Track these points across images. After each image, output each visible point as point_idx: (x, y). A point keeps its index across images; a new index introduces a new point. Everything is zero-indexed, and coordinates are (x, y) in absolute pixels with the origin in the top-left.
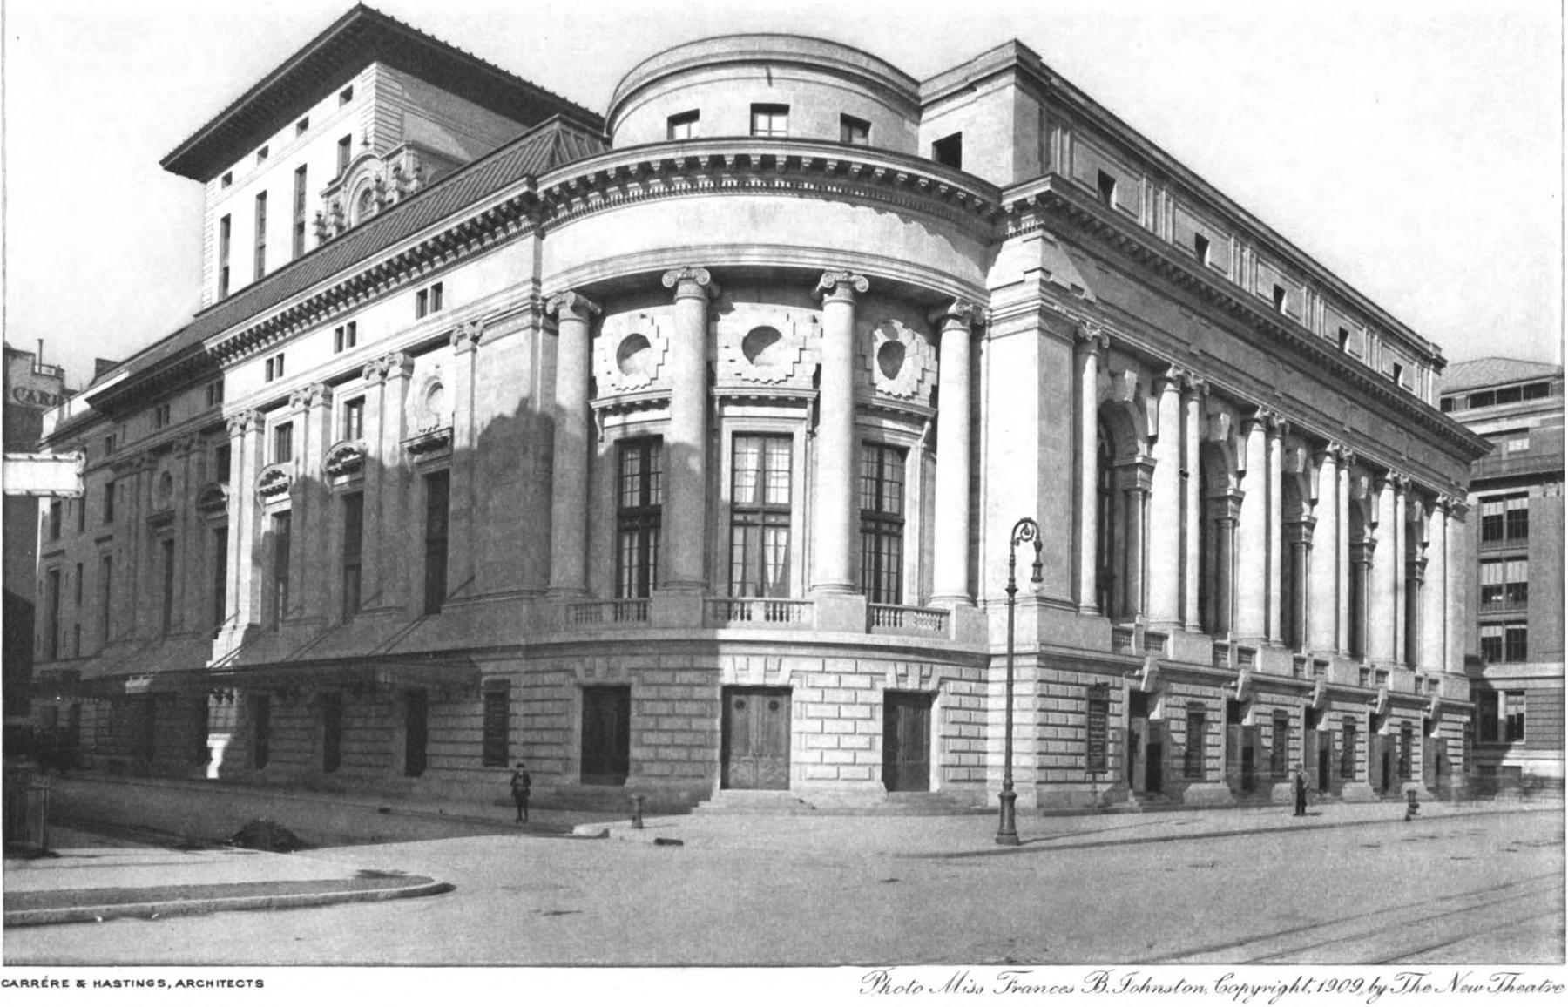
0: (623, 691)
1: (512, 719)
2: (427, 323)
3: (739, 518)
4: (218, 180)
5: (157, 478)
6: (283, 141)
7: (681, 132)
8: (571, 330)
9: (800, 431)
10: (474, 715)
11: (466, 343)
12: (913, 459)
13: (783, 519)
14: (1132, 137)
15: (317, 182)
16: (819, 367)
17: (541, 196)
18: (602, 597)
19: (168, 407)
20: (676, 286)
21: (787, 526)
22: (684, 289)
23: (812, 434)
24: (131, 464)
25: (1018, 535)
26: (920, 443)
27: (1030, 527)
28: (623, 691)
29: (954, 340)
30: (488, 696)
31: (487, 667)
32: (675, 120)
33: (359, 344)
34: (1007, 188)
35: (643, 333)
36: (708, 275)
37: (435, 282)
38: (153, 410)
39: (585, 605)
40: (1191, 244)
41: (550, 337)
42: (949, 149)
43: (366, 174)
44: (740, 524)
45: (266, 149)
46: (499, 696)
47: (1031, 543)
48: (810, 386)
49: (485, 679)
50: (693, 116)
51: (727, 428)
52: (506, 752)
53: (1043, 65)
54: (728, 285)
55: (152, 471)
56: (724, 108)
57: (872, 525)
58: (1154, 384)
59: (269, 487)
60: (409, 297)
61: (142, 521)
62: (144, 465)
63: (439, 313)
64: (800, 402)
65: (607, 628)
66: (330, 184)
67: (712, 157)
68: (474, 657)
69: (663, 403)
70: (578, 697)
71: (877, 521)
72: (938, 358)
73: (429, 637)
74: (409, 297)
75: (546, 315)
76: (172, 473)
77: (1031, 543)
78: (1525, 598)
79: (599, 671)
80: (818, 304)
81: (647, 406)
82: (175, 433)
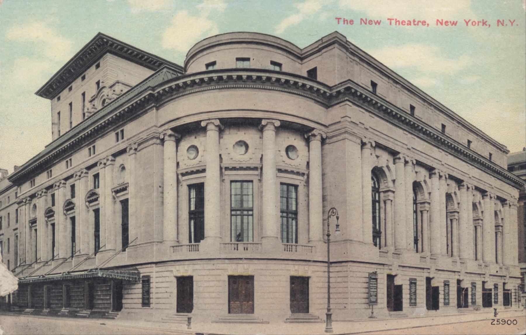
0: (191, 278)
1: (151, 289)
2: (119, 144)
3: (233, 213)
4: (56, 99)
5: (32, 206)
6: (77, 84)
7: (211, 68)
8: (170, 144)
9: (255, 179)
10: (138, 289)
11: (132, 151)
12: (301, 189)
13: (250, 213)
14: (384, 68)
15: (88, 98)
16: (262, 155)
17: (156, 95)
18: (184, 243)
19: (34, 180)
20: (207, 126)
21: (252, 215)
22: (210, 127)
23: (260, 180)
24: (22, 202)
25: (330, 214)
26: (303, 183)
27: (334, 211)
28: (191, 278)
29: (315, 144)
30: (143, 281)
31: (141, 271)
32: (208, 65)
33: (96, 153)
34: (333, 87)
35: (196, 145)
36: (218, 121)
37: (121, 129)
38: (30, 181)
39: (177, 246)
40: (409, 108)
41: (54, 122)
42: (312, 73)
43: (103, 94)
44: (234, 215)
45: (71, 87)
46: (146, 281)
47: (335, 217)
48: (259, 162)
49: (141, 275)
50: (214, 63)
51: (227, 179)
52: (149, 301)
53: (347, 41)
54: (228, 124)
55: (30, 203)
56: (226, 59)
57: (285, 215)
58: (394, 160)
59: (68, 207)
60: (113, 135)
61: (27, 222)
62: (27, 202)
63: (123, 140)
64: (256, 169)
65: (184, 253)
66: (92, 97)
67: (218, 77)
68: (138, 267)
69: (204, 171)
70: (175, 281)
71: (287, 213)
72: (309, 151)
73: (124, 259)
74: (113, 135)
75: (160, 139)
76: (37, 205)
77: (335, 217)
78: (250, 296)
79: (183, 270)
80: (261, 130)
81: (198, 172)
82: (37, 189)
